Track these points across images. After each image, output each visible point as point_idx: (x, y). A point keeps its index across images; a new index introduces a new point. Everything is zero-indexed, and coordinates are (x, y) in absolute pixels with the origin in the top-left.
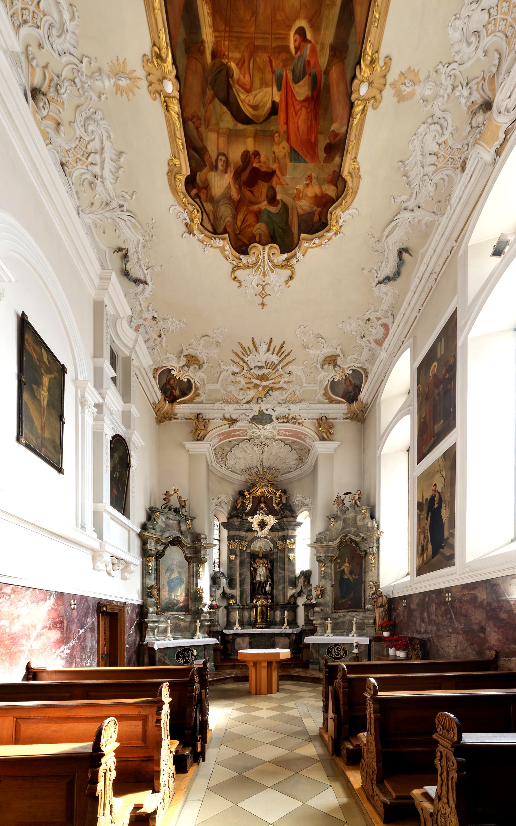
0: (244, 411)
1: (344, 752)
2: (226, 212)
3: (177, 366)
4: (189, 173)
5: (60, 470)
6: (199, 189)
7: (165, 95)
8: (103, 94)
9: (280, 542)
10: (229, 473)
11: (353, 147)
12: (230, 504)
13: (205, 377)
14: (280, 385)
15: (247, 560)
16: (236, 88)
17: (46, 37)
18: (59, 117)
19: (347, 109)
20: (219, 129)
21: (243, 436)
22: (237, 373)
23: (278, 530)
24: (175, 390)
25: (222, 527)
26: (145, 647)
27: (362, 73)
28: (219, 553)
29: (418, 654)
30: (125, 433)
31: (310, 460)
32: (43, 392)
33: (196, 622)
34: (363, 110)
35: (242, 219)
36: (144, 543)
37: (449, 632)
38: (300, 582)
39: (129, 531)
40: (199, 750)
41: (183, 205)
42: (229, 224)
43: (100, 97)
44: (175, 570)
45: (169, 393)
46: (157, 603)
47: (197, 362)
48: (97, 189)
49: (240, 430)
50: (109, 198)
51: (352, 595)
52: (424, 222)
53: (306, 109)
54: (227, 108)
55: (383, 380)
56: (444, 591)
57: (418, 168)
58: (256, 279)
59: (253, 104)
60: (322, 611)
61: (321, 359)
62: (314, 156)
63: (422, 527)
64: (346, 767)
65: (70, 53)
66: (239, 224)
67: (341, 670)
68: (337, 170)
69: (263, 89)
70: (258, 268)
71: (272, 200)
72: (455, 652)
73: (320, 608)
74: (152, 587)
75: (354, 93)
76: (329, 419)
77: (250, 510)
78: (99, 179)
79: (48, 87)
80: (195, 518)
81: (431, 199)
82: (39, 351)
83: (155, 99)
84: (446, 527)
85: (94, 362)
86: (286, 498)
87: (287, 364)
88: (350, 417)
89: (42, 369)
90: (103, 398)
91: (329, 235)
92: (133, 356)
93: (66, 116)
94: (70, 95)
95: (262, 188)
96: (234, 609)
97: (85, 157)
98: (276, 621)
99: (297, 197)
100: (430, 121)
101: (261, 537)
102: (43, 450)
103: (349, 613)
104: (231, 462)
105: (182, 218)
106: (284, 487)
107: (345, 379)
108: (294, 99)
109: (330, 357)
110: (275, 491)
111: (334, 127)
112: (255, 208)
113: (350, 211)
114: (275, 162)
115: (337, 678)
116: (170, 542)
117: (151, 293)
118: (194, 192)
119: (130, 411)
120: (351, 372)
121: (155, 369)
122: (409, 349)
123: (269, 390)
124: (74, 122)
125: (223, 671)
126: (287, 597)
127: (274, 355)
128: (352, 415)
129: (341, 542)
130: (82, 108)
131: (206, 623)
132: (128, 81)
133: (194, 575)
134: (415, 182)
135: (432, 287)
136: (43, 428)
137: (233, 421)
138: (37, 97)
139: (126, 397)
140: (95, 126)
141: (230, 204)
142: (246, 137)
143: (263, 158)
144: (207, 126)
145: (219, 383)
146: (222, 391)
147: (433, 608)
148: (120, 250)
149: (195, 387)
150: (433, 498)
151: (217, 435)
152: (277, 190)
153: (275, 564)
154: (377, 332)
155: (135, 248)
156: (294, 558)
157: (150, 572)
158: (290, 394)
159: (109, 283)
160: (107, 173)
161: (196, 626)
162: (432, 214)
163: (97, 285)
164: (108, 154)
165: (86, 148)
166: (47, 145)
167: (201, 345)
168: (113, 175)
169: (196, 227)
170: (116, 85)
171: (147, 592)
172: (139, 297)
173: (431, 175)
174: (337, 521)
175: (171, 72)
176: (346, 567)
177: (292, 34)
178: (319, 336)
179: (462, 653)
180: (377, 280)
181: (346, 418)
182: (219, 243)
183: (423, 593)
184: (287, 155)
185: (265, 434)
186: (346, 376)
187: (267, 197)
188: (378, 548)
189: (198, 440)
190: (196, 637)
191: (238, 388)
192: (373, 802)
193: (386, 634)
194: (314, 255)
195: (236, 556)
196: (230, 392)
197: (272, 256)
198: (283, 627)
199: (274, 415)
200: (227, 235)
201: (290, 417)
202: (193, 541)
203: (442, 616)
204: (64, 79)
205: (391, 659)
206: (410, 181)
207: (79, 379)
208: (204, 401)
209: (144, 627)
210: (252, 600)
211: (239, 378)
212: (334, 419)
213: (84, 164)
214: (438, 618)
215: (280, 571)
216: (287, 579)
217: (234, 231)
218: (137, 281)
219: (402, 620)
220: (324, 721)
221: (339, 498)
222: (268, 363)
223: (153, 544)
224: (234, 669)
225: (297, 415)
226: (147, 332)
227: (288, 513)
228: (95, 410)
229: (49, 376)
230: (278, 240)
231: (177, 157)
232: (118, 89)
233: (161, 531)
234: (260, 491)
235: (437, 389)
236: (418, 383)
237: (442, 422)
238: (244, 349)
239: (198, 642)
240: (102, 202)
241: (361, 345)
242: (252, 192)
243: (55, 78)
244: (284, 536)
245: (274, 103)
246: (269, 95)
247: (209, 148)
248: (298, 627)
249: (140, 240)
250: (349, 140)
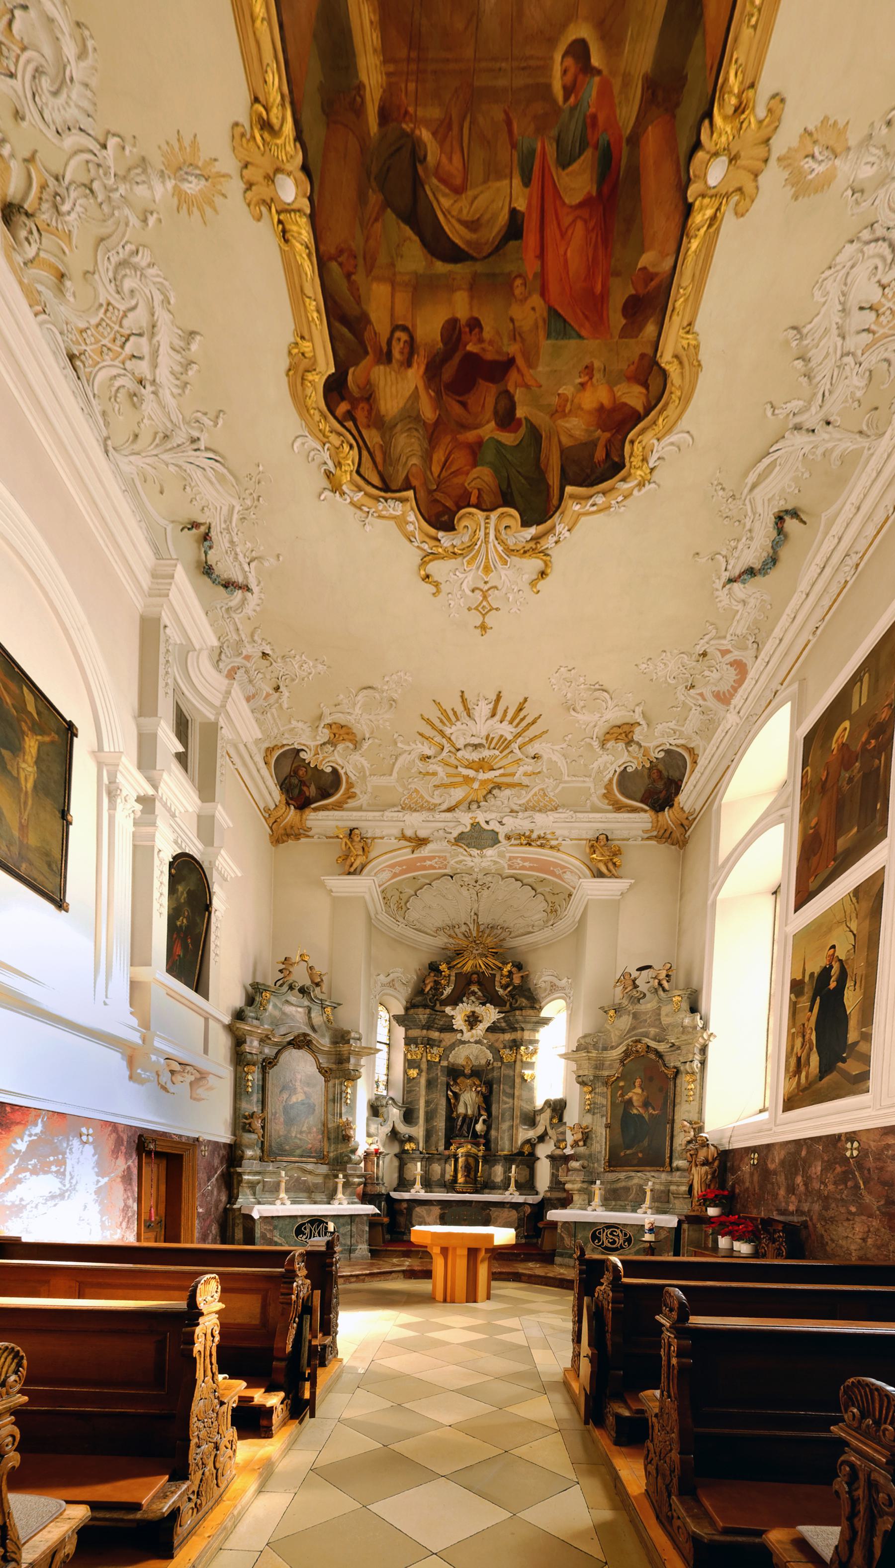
0: (441, 825)
1: (611, 1420)
2: (408, 447)
3: (312, 744)
4: (332, 370)
5: (60, 904)
6: (354, 402)
7: (279, 208)
8: (152, 213)
9: (507, 1051)
10: (411, 933)
11: (686, 300)
12: (411, 985)
13: (366, 764)
15: (443, 1079)
16: (432, 187)
17: (29, 95)
18: (62, 262)
20: (394, 275)
21: (440, 868)
22: (429, 757)
23: (503, 1031)
24: (308, 787)
25: (394, 1023)
26: (237, 1213)
27: (715, 135)
28: (388, 1065)
29: (779, 1249)
30: (202, 854)
31: (574, 910)
32: (23, 765)
33: (337, 1176)
34: (714, 218)
35: (443, 459)
36: (238, 1042)
37: (850, 1213)
38: (544, 1120)
39: (206, 1020)
40: (307, 1395)
41: (321, 436)
42: (414, 470)
43: (145, 221)
44: (299, 1090)
45: (296, 791)
46: (262, 1142)
47: (350, 737)
48: (144, 406)
49: (434, 857)
50: (169, 425)
51: (646, 1143)
52: (836, 453)
53: (585, 222)
54: (412, 228)
55: (728, 767)
56: (843, 1138)
57: (834, 338)
58: (470, 578)
59: (468, 218)
60: (584, 1167)
61: (600, 730)
63: (799, 1023)
64: (614, 1448)
65: (81, 129)
66: (436, 469)
67: (611, 1269)
68: (649, 351)
69: (490, 183)
70: (474, 558)
71: (507, 418)
72: (861, 1248)
73: (581, 1162)
74: (252, 1116)
75: (695, 182)
76: (612, 840)
77: (449, 996)
78: (148, 386)
79: (37, 201)
80: (339, 1004)
81: (856, 404)
82: (18, 692)
83: (259, 219)
84: (853, 1023)
85: (138, 726)
86: (522, 977)
87: (531, 740)
88: (655, 837)
89: (23, 724)
90: (155, 787)
91: (625, 486)
92: (221, 723)
93: (76, 260)
94: (83, 216)
95: (486, 396)
96: (413, 1159)
97: (118, 343)
98: (493, 1182)
99: (559, 412)
100: (866, 235)
101: (469, 1042)
102: (24, 866)
103: (639, 1174)
104: (414, 914)
105: (318, 460)
106: (518, 959)
107: (649, 769)
108: (558, 202)
109: (619, 727)
110: (500, 965)
111: (646, 260)
112: (470, 436)
113: (673, 438)
114: (515, 339)
115: (602, 1284)
116: (290, 1043)
117: (258, 608)
118: (343, 407)
119: (213, 816)
120: (662, 755)
121: (268, 749)
122: (789, 704)
123: (493, 788)
124: (94, 273)
125: (386, 1259)
126: (516, 1142)
127: (505, 723)
128: (662, 831)
129: (627, 1053)
130: (108, 243)
131: (356, 1180)
132: (203, 182)
133: (336, 1099)
134: (824, 372)
135: (846, 582)
136: (23, 828)
137: (420, 842)
138: (14, 219)
139: (206, 789)
140: (137, 280)
141: (416, 430)
142: (452, 289)
143: (488, 332)
144: (369, 271)
146: (400, 790)
147: (817, 1169)
148: (195, 525)
149: (347, 782)
150: (826, 972)
151: (387, 867)
152: (516, 398)
153: (495, 1086)
154: (720, 675)
155: (225, 522)
156: (533, 1078)
157: (250, 1090)
158: (535, 795)
159: (171, 584)
160: (163, 374)
161: (337, 1183)
162: (857, 436)
163: (145, 587)
164: (166, 336)
165: (121, 326)
166: (36, 315)
167: (359, 705)
168: (178, 379)
169: (346, 478)
170: (178, 192)
171: (241, 1123)
172: (234, 615)
173: (859, 352)
174: (620, 1016)
175: (291, 157)
176: (636, 1094)
177: (558, 57)
178: (597, 686)
179: (876, 1252)
180: (725, 576)
181: (648, 838)
182: (395, 508)
183: (797, 1142)
184: (541, 324)
185: (483, 864)
186: (651, 762)
187: (496, 413)
188: (703, 1063)
189: (349, 874)
190: (336, 1202)
191: (431, 785)
192: (669, 1528)
193: (712, 1212)
194: (590, 529)
195: (421, 1071)
196: (416, 791)
197: (503, 532)
198: (507, 1193)
199: (502, 832)
200: (411, 493)
201: (534, 836)
202: (335, 1043)
203: (835, 1183)
204: (70, 184)
205: (720, 1255)
206: (812, 370)
207: (106, 749)
208: (364, 807)
209: (235, 1181)
210: (447, 1146)
211: (433, 767)
212: (623, 840)
213: (117, 357)
214: (826, 1185)
215: (505, 1098)
216: (517, 1113)
217: (425, 483)
218: (228, 585)
219: (748, 1188)
220: (574, 1356)
221: (627, 977)
222: (493, 738)
223: (256, 1043)
224: (408, 1257)
225: (548, 832)
226: (251, 681)
227: (524, 1002)
228: (138, 807)
229: (39, 738)
230: (518, 499)
231: (307, 337)
232: (183, 201)
233: (272, 1023)
234: (470, 963)
235: (847, 770)
236: (805, 764)
237: (855, 829)
238: (444, 712)
239: (339, 1209)
240: (156, 433)
241: (684, 703)
242: (464, 405)
243: (52, 182)
244: (514, 1041)
245: (513, 212)
247: (373, 317)
248: (537, 1193)
249: (233, 507)
250: (679, 286)
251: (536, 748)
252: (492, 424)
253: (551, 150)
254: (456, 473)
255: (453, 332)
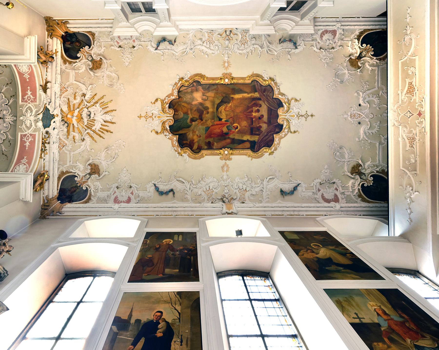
3: (92, 52)
13: (80, 71)
14: (72, 133)
19: (219, 147)
24: (70, 44)
45: (69, 39)
58: (156, 112)
62: (207, 137)
66: (183, 104)
71: (192, 120)
123: (68, 124)
127: (101, 126)
134: (200, 185)
143: (207, 115)
145: (76, 82)
146: (67, 84)
149: (72, 62)
154: (123, 195)
158: (64, 142)
163: (176, 22)
177: (237, 124)
180: (156, 183)
181: (44, 199)
182: (176, 93)
186: (80, 186)
187: (194, 118)
191: (69, 97)
196: (67, 91)
199: (50, 129)
232: (224, 62)
242: (195, 111)
246: (224, 117)
247: (209, 93)
251: (88, 139)
252: (191, 117)
253: (228, 125)
254: (182, 109)
255: (207, 108)
